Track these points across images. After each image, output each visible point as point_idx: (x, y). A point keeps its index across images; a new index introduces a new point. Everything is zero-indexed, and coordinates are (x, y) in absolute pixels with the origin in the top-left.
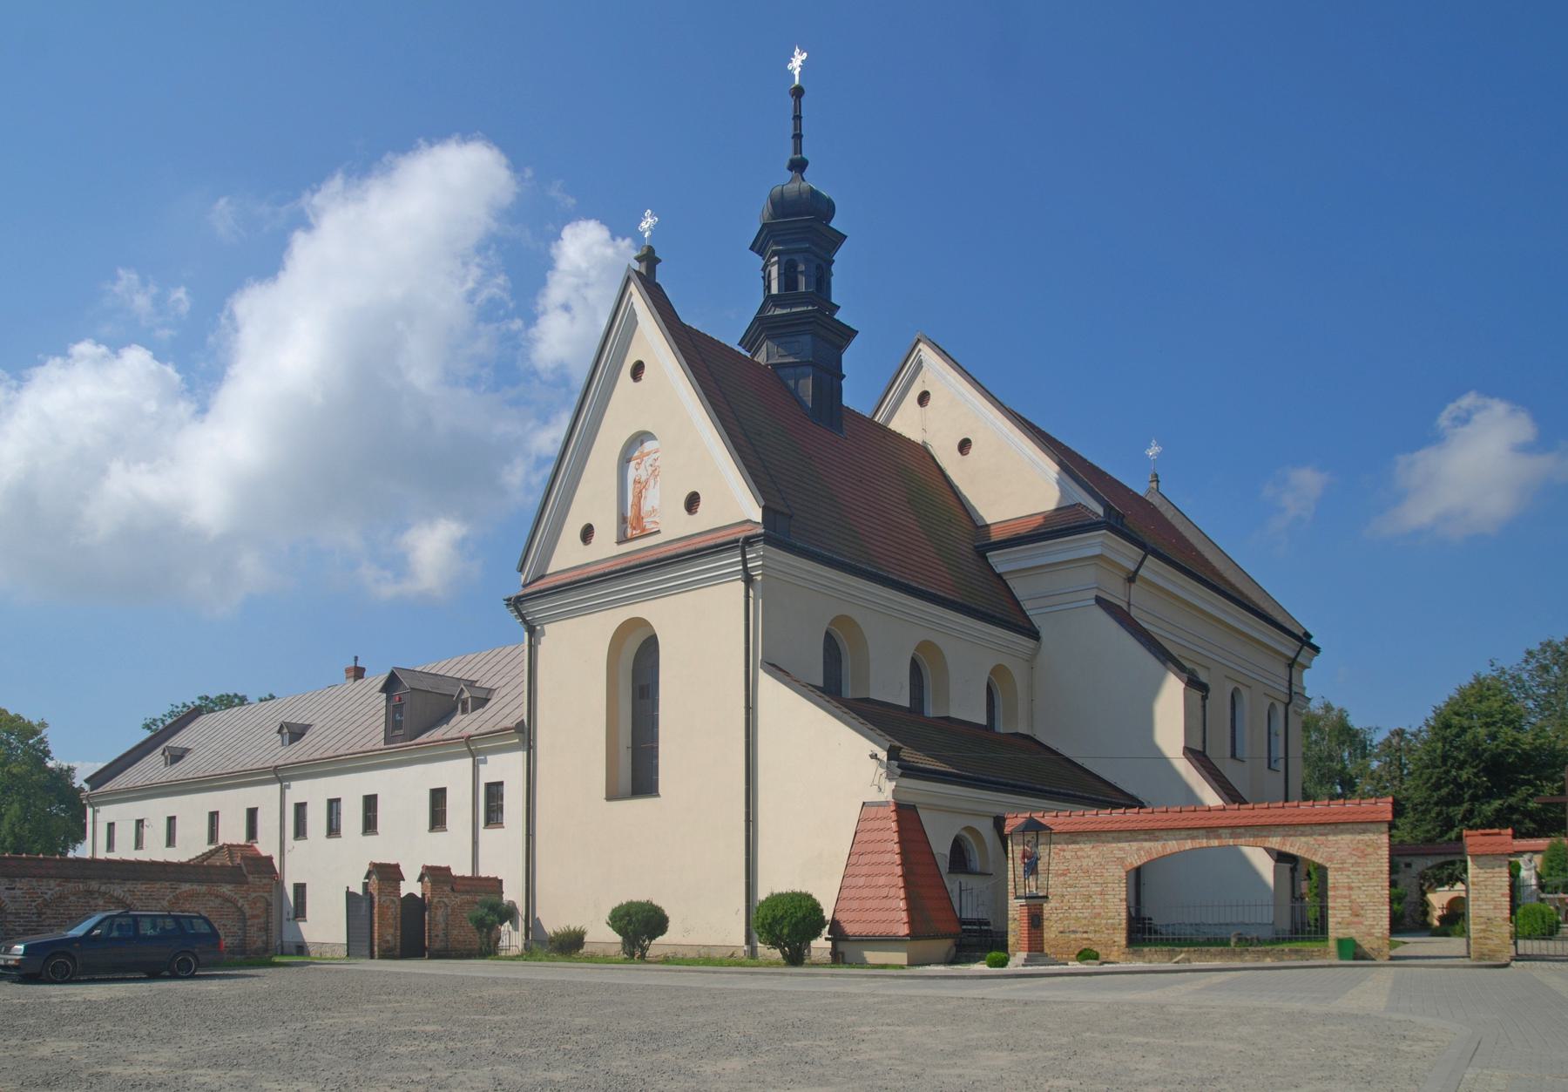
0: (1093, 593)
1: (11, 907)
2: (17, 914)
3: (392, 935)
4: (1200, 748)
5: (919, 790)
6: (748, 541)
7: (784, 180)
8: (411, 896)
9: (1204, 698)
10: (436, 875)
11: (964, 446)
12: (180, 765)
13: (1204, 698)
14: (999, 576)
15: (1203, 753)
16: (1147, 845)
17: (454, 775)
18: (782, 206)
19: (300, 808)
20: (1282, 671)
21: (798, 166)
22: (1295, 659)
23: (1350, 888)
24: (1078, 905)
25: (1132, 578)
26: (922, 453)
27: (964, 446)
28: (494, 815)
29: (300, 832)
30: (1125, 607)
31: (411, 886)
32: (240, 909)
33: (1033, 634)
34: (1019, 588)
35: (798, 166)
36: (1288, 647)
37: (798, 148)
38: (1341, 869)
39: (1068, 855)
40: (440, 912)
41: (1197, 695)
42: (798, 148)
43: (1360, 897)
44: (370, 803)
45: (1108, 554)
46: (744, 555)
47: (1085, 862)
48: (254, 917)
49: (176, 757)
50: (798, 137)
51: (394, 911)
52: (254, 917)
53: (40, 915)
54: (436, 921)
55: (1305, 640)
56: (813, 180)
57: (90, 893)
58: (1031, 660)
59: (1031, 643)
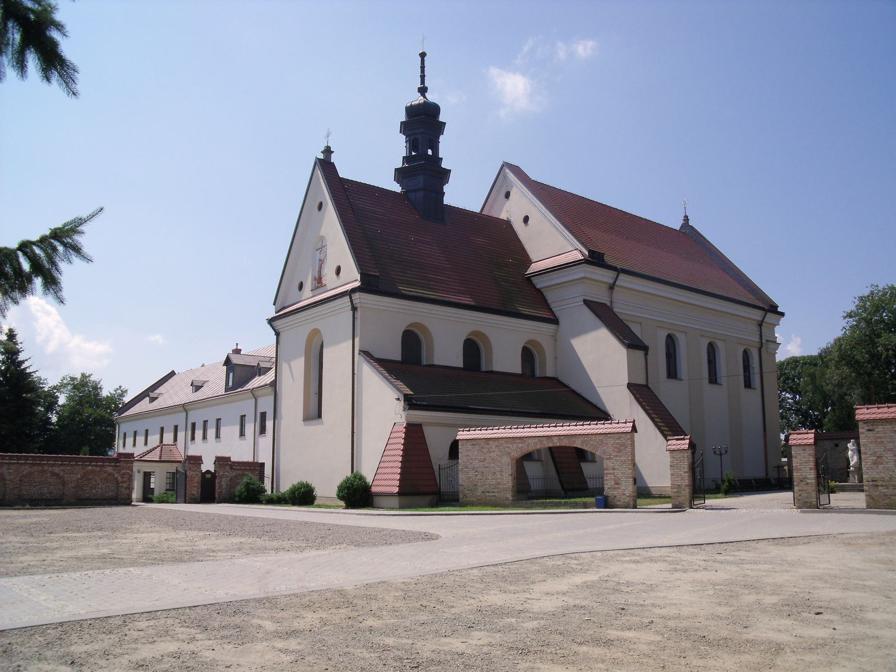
0: (582, 298)
1: (7, 478)
2: (11, 481)
3: (195, 491)
4: (643, 382)
5: (420, 416)
6: (354, 290)
7: (418, 99)
8: (208, 472)
9: (646, 354)
10: (221, 461)
11: (526, 220)
12: (155, 402)
13: (646, 354)
14: (539, 290)
15: (646, 386)
16: (520, 445)
17: (247, 407)
18: (411, 111)
19: (194, 425)
20: (756, 329)
21: (423, 90)
22: (762, 321)
23: (614, 469)
24: (490, 478)
25: (612, 287)
26: (508, 224)
27: (526, 220)
28: (263, 430)
29: (193, 438)
30: (608, 304)
31: (208, 465)
32: (116, 479)
33: (555, 321)
34: (550, 297)
35: (423, 90)
36: (757, 315)
37: (423, 82)
38: (610, 459)
39: (485, 450)
40: (224, 479)
41: (641, 354)
42: (423, 82)
43: (618, 473)
44: (218, 420)
45: (588, 275)
46: (351, 298)
47: (493, 454)
48: (123, 482)
49: (153, 400)
50: (423, 77)
51: (198, 479)
52: (123, 482)
53: (21, 481)
54: (222, 485)
55: (773, 309)
56: (431, 97)
57: (45, 471)
58: (555, 337)
59: (552, 327)
